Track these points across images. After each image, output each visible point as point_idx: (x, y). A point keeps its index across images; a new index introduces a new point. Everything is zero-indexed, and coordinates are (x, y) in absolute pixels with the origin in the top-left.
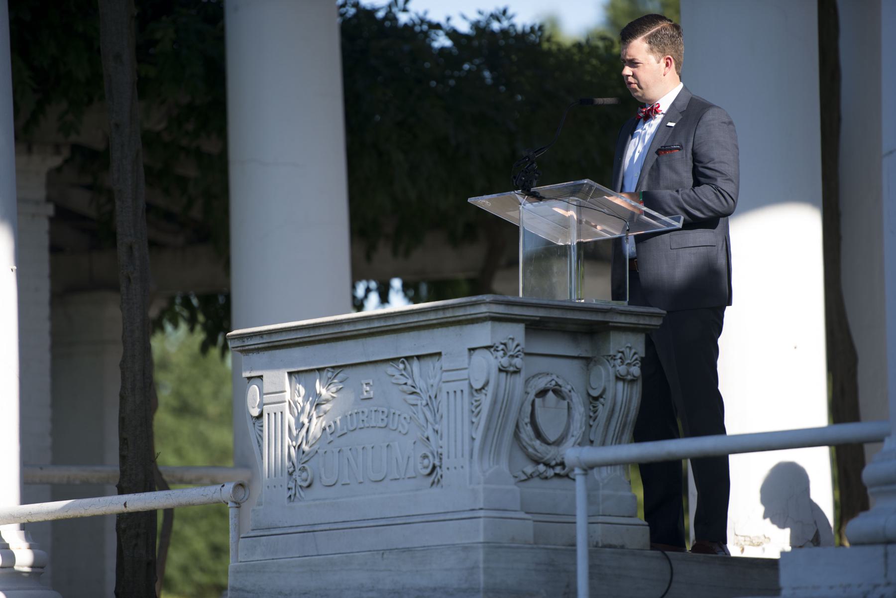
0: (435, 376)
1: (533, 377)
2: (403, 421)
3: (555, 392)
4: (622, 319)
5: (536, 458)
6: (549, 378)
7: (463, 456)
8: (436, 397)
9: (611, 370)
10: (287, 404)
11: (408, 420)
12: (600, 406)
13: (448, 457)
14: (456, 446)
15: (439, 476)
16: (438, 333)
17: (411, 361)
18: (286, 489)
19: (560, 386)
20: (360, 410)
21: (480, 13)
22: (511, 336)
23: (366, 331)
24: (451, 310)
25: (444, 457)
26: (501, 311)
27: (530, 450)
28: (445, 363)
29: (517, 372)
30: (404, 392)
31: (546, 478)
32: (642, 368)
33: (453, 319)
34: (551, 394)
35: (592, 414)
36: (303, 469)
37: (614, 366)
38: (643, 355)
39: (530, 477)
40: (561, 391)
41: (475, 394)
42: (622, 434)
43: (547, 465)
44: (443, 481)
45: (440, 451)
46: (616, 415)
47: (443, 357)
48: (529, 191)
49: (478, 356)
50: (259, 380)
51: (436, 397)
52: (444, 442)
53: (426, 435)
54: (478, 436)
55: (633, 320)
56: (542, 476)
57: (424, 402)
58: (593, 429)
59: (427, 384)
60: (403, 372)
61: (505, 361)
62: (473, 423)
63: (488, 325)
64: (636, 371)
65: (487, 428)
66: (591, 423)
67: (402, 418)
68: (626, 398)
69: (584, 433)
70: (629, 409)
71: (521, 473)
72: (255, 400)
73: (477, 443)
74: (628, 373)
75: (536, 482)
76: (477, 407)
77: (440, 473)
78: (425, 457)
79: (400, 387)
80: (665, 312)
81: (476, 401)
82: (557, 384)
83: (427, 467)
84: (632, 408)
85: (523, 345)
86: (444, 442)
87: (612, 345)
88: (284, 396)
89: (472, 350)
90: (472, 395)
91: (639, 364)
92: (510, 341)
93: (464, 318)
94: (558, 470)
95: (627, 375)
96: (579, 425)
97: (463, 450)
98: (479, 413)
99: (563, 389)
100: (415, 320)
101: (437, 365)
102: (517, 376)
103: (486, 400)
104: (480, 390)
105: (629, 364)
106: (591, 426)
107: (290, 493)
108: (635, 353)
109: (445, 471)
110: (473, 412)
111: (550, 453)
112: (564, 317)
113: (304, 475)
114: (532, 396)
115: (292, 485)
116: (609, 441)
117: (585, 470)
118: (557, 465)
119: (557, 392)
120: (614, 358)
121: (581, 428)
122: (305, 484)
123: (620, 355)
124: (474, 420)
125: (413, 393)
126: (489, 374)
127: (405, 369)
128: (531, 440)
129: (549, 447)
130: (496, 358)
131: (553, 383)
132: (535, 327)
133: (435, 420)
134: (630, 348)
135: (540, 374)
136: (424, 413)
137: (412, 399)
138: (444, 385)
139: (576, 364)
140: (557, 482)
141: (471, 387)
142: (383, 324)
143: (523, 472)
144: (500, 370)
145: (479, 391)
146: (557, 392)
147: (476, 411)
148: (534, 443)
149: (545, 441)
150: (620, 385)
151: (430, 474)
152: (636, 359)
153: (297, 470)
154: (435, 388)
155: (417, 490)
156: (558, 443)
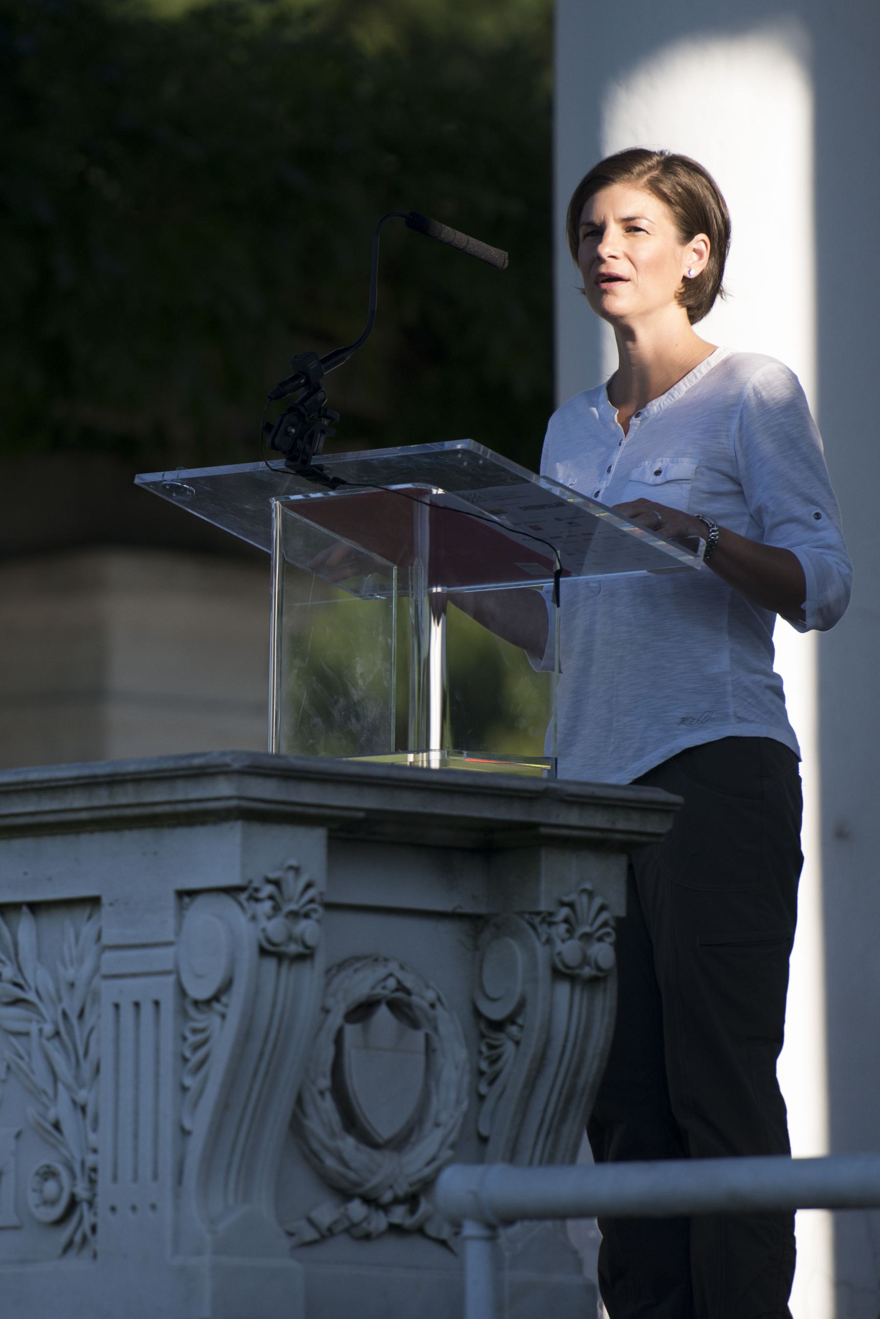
0: (81, 960)
3: (395, 1006)
4: (573, 817)
7: (155, 1176)
8: (81, 1015)
9: (542, 953)
12: (509, 1047)
13: (115, 1178)
14: (136, 1149)
15: (86, 1227)
16: (93, 845)
19: (408, 992)
22: (293, 862)
24: (130, 787)
26: (268, 795)
27: (330, 1162)
28: (111, 925)
29: (306, 956)
31: (367, 1237)
32: (618, 947)
33: (137, 811)
34: (383, 1013)
35: (484, 1066)
37: (549, 941)
38: (622, 912)
39: (327, 1235)
40: (409, 1006)
41: (192, 1011)
42: (563, 1120)
43: (371, 1201)
45: (91, 1159)
46: (550, 1070)
47: (106, 909)
48: (305, 462)
49: (204, 916)
51: (81, 1015)
52: (102, 1138)
53: (51, 1115)
54: (200, 1123)
57: (48, 1029)
58: (488, 1105)
59: (56, 980)
61: (276, 928)
62: (184, 1089)
63: (235, 831)
64: (604, 953)
65: (224, 1106)
66: (483, 1089)
68: (574, 1025)
70: (583, 1053)
71: (303, 1224)
73: (196, 1145)
74: (585, 960)
75: (342, 1246)
76: (197, 1047)
77: (88, 1219)
78: (48, 1174)
81: (195, 1031)
82: (401, 987)
83: (52, 1203)
84: (590, 1052)
86: (102, 1138)
87: (543, 886)
89: (186, 895)
90: (183, 1014)
91: (612, 939)
92: (291, 875)
93: (167, 808)
94: (399, 1215)
95: (581, 966)
96: (453, 1096)
97: (156, 1162)
99: (415, 999)
100: (30, 808)
101: (88, 930)
103: (223, 1033)
104: (208, 1002)
105: (587, 937)
106: (482, 1098)
108: (602, 908)
110: (185, 1060)
112: (428, 810)
114: (336, 1019)
117: (491, 1227)
119: (400, 1007)
120: (548, 919)
121: (458, 1102)
123: (564, 912)
124: (188, 1081)
125: (17, 1002)
126: (233, 961)
128: (333, 1135)
129: (377, 1155)
131: (392, 983)
132: (353, 836)
133: (77, 1077)
134: (591, 894)
135: (358, 959)
138: (105, 983)
139: (446, 928)
140: (393, 1247)
141: (182, 992)
143: (311, 1222)
144: (263, 952)
146: (400, 1007)
148: (340, 1144)
149: (367, 1139)
150: (563, 990)
152: (605, 924)
156: (400, 1142)
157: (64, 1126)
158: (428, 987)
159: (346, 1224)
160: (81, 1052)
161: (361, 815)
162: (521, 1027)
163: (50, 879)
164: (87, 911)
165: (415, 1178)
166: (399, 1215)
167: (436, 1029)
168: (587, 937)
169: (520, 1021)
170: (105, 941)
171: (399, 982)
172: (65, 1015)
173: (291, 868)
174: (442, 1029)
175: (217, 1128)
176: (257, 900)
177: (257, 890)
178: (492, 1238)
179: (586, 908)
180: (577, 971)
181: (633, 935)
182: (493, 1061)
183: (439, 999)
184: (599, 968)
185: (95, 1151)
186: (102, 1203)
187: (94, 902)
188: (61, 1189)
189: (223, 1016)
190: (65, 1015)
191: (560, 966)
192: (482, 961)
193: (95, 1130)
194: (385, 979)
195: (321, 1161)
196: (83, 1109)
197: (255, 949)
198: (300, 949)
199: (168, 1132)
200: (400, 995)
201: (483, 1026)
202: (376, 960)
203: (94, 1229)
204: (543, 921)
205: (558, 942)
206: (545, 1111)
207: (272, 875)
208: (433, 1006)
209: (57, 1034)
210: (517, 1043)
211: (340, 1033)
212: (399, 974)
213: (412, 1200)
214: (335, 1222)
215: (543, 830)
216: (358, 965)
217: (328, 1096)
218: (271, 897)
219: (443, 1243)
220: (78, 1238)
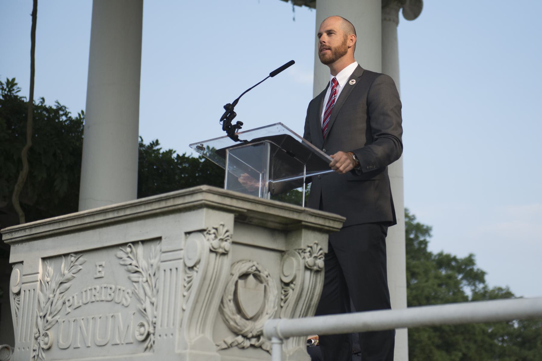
0: (155, 257)
1: (238, 262)
2: (127, 296)
3: (255, 276)
5: (236, 331)
6: (251, 264)
8: (154, 275)
10: (39, 283)
11: (131, 294)
13: (161, 326)
15: (152, 342)
17: (136, 245)
18: (32, 351)
19: (259, 271)
20: (93, 287)
21: (200, 148)
22: (222, 223)
23: (102, 222)
24: (172, 200)
25: (158, 326)
27: (232, 323)
28: (164, 245)
29: (225, 254)
30: (129, 271)
31: (243, 348)
32: (325, 261)
34: (251, 277)
35: (283, 297)
36: (46, 335)
37: (304, 258)
39: (230, 346)
40: (260, 276)
41: (188, 271)
43: (245, 337)
44: (155, 347)
45: (154, 320)
47: (163, 240)
50: (21, 264)
51: (154, 275)
53: (144, 306)
55: (321, 222)
56: (240, 346)
57: (145, 279)
58: (284, 309)
60: (130, 255)
61: (216, 243)
62: (184, 296)
64: (320, 263)
65: (196, 302)
66: (282, 304)
67: (126, 292)
68: (313, 285)
69: (276, 311)
70: (313, 294)
72: (17, 280)
73: (187, 313)
74: (315, 265)
75: (235, 350)
76: (189, 282)
79: (126, 267)
80: (345, 218)
81: (188, 277)
82: (257, 270)
83: (142, 334)
85: (231, 232)
87: (303, 241)
88: (37, 277)
89: (188, 233)
94: (254, 341)
96: (272, 305)
98: (190, 288)
99: (261, 274)
102: (225, 258)
103: (197, 276)
106: (282, 307)
107: (35, 354)
108: (321, 249)
109: (157, 338)
110: (185, 287)
111: (250, 327)
113: (46, 339)
114: (236, 278)
115: (36, 347)
117: (281, 339)
118: (253, 337)
120: (304, 251)
121: (274, 307)
122: (45, 347)
123: (309, 249)
125: (137, 272)
127: (131, 252)
128: (233, 314)
129: (247, 322)
130: (208, 240)
131: (254, 268)
133: (152, 294)
134: (317, 244)
136: (144, 288)
137: (135, 277)
139: (272, 254)
140: (251, 351)
142: (116, 215)
143: (225, 342)
144: (211, 251)
145: (191, 268)
146: (257, 276)
147: (188, 286)
150: (308, 273)
151: (144, 340)
152: (321, 254)
153: (41, 335)
154: (155, 267)
155: (133, 354)
156: (254, 319)
157: (147, 310)
158: (266, 270)
159: (236, 343)
160: (154, 286)
161: (245, 211)
162: (295, 285)
163: (147, 233)
164: (158, 242)
165: (259, 330)
166: (254, 341)
167: (268, 284)
168: (316, 257)
169: (294, 283)
170: (163, 250)
171: (257, 268)
172: (150, 275)
173: (221, 225)
174: (270, 284)
175: (194, 309)
176: (210, 234)
177: (210, 231)
178: (282, 343)
179: (316, 249)
180: (312, 268)
181: (331, 257)
182: (286, 296)
183: (269, 274)
184: (319, 267)
185: (156, 317)
186: (157, 334)
187: (159, 239)
188: (145, 330)
189: (197, 272)
190: (150, 275)
191: (307, 266)
192: (283, 265)
193: (156, 311)
194: (252, 267)
195: (229, 323)
196: (153, 304)
197: (208, 250)
198: (224, 251)
199: (179, 310)
200: (257, 272)
201: (283, 285)
202: (250, 261)
203: (154, 342)
204: (302, 252)
205: (307, 258)
206: (301, 311)
207: (215, 227)
208: (267, 276)
209: (147, 281)
210: (293, 290)
211: (237, 282)
212: (257, 265)
213: (258, 337)
214: (233, 343)
215: (303, 223)
216: (244, 262)
217: (232, 301)
218: (214, 233)
219: (268, 351)
220: (149, 346)
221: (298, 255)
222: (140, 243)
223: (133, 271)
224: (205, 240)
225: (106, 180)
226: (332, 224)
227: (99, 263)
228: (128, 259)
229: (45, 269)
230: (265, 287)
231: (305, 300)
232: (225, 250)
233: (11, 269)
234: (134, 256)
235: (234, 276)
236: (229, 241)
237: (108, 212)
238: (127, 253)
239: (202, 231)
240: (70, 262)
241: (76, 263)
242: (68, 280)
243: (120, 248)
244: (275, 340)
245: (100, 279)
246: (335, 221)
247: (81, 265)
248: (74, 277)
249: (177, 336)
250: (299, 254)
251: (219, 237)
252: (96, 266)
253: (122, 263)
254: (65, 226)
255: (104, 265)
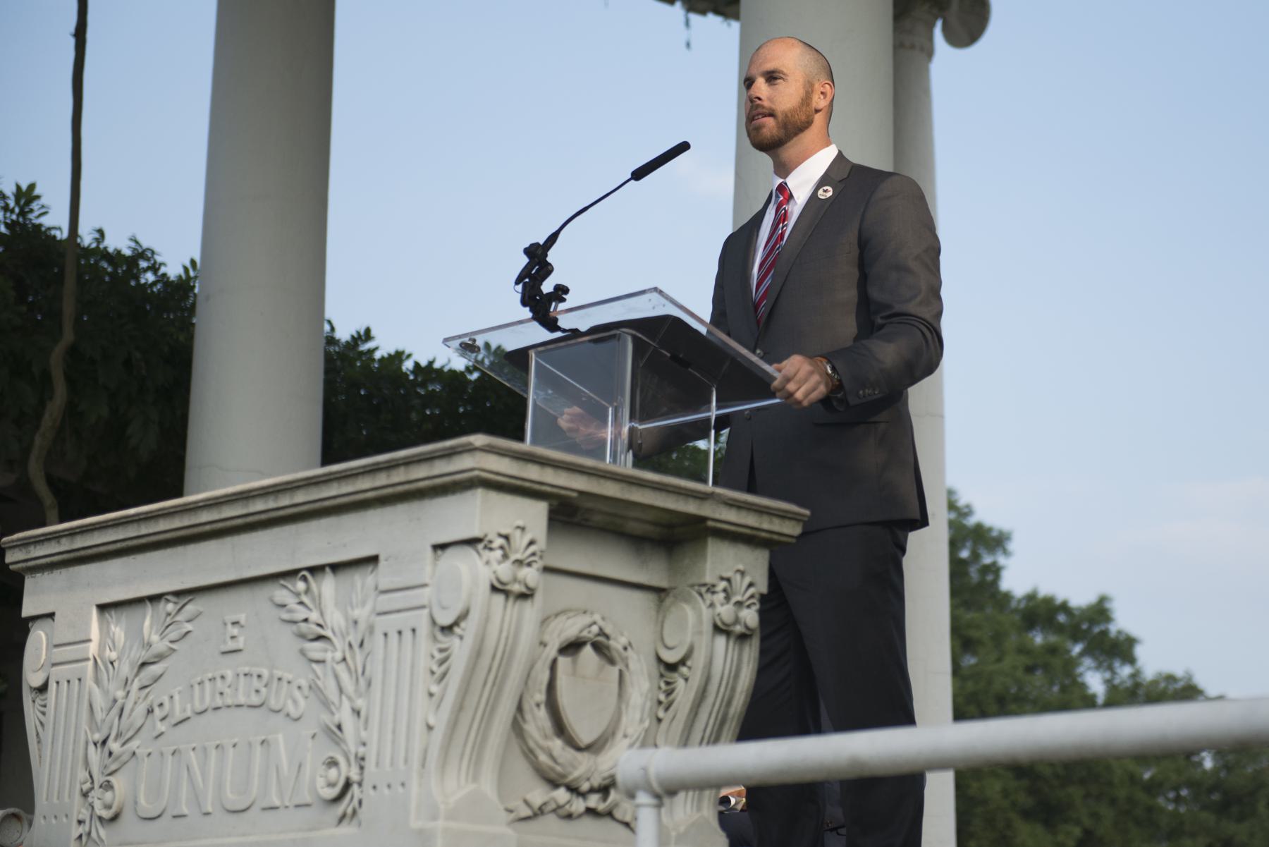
0: (364, 603)
1: (557, 615)
2: (297, 694)
3: (597, 647)
5: (552, 776)
6: (587, 620)
8: (361, 645)
10: (91, 663)
11: (306, 690)
13: (377, 764)
15: (355, 802)
17: (319, 576)
18: (75, 823)
19: (607, 637)
20: (218, 674)
22: (520, 523)
23: (239, 521)
24: (402, 469)
25: (370, 765)
27: (543, 758)
28: (384, 575)
29: (526, 595)
30: (302, 636)
31: (569, 816)
32: (761, 613)
34: (588, 650)
35: (662, 697)
36: (108, 786)
37: (712, 605)
39: (539, 812)
40: (608, 648)
41: (439, 636)
43: (573, 790)
44: (363, 813)
45: (362, 750)
47: (382, 562)
50: (50, 620)
51: (361, 645)
53: (336, 719)
55: (750, 520)
56: (561, 812)
57: (339, 655)
58: (664, 725)
60: (305, 599)
61: (505, 571)
62: (431, 695)
64: (750, 617)
65: (460, 708)
66: (661, 714)
67: (294, 686)
68: (732, 669)
69: (647, 731)
70: (733, 689)
72: (39, 657)
73: (438, 735)
74: (737, 621)
75: (551, 821)
76: (442, 662)
79: (294, 627)
80: (807, 512)
81: (441, 650)
82: (601, 632)
83: (331, 785)
85: (542, 543)
87: (709, 565)
88: (88, 649)
89: (440, 547)
94: (594, 801)
96: (638, 716)
98: (444, 675)
99: (612, 643)
102: (527, 605)
103: (460, 648)
106: (659, 720)
107: (81, 830)
108: (751, 585)
109: (368, 794)
110: (433, 673)
111: (584, 768)
113: (108, 795)
114: (552, 651)
115: (85, 814)
116: (697, 734)
117: (657, 796)
118: (592, 790)
120: (711, 589)
121: (642, 721)
122: (106, 814)
123: (723, 584)
125: (320, 638)
127: (307, 591)
128: (546, 737)
129: (579, 755)
130: (488, 563)
131: (595, 629)
133: (356, 691)
134: (743, 573)
136: (336, 677)
137: (315, 649)
139: (637, 596)
140: (589, 823)
142: (271, 504)
143: (526, 802)
144: (494, 589)
145: (448, 629)
146: (601, 648)
147: (439, 671)
150: (721, 641)
151: (338, 799)
152: (752, 596)
153: (96, 786)
154: (362, 626)
155: (310, 830)
156: (594, 748)
157: (344, 727)
158: (622, 635)
159: (553, 806)
160: (360, 670)
161: (574, 495)
162: (690, 668)
163: (345, 546)
164: (370, 568)
165: (606, 774)
166: (594, 801)
167: (627, 666)
168: (739, 604)
169: (689, 663)
170: (382, 587)
171: (601, 629)
172: (350, 645)
173: (518, 527)
174: (631, 666)
175: (453, 725)
176: (491, 549)
177: (491, 542)
178: (659, 806)
179: (740, 584)
180: (732, 628)
181: (774, 604)
182: (669, 693)
183: (630, 644)
184: (747, 627)
185: (364, 744)
186: (367, 785)
187: (373, 560)
188: (340, 774)
189: (461, 638)
190: (350, 645)
191: (719, 624)
192: (663, 622)
193: (366, 729)
194: (590, 626)
195: (536, 757)
196: (358, 713)
197: (488, 587)
198: (523, 590)
199: (419, 728)
200: (601, 639)
201: (662, 669)
202: (585, 612)
203: (360, 802)
204: (708, 590)
205: (718, 605)
206: (705, 731)
207: (504, 532)
208: (625, 649)
209: (344, 659)
210: (686, 680)
211: (554, 662)
212: (601, 623)
213: (604, 790)
214: (545, 804)
215: (710, 523)
216: (571, 614)
217: (543, 707)
218: (502, 548)
219: (627, 825)
220: (350, 811)
221: (699, 598)
222: (328, 569)
223: (311, 637)
224: (480, 563)
225: (248, 423)
226: (777, 526)
227: (231, 618)
228: (300, 608)
229: (105, 631)
230: (621, 672)
231: (714, 705)
232: (527, 587)
233: (26, 632)
234: (313, 600)
235: (548, 648)
236: (535, 566)
237: (254, 497)
238: (298, 594)
239: (472, 542)
240: (164, 616)
241: (178, 618)
242: (160, 657)
243: (282, 582)
244: (643, 798)
245: (234, 655)
246: (783, 519)
247: (189, 621)
248: (174, 650)
249: (414, 789)
250: (701, 595)
251: (514, 557)
252: (225, 624)
253: (286, 616)
254: (151, 531)
255: (243, 622)
